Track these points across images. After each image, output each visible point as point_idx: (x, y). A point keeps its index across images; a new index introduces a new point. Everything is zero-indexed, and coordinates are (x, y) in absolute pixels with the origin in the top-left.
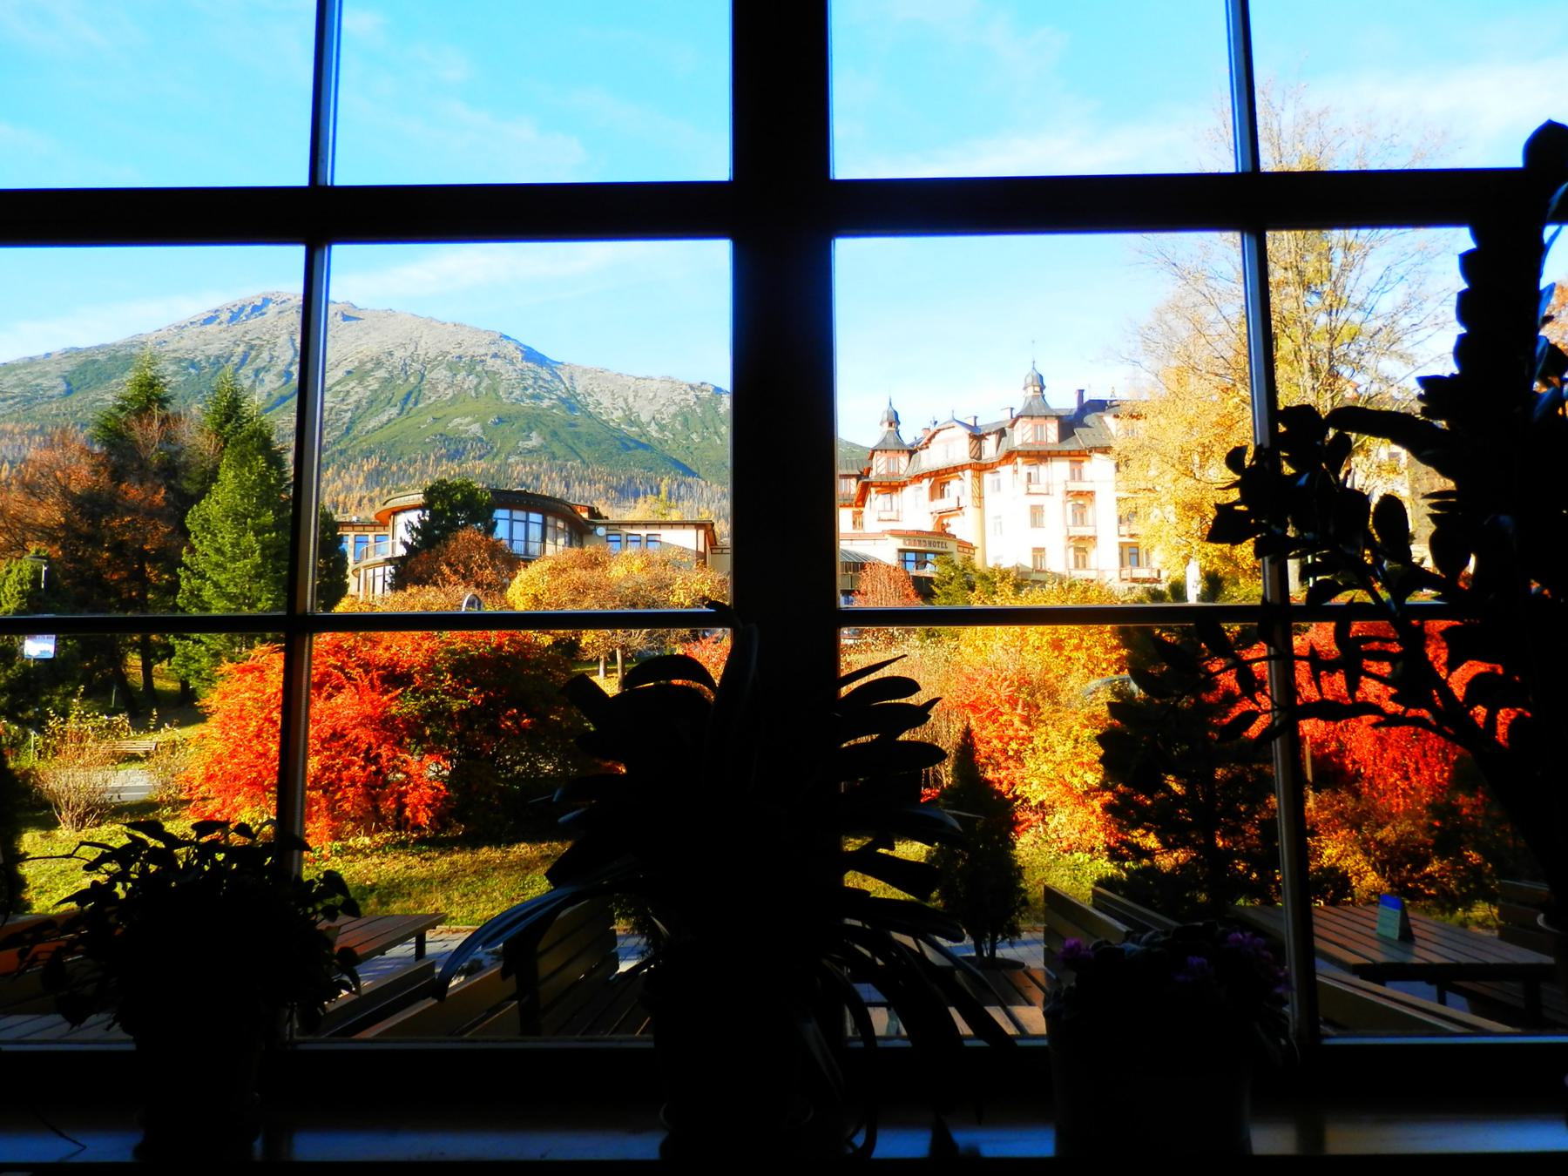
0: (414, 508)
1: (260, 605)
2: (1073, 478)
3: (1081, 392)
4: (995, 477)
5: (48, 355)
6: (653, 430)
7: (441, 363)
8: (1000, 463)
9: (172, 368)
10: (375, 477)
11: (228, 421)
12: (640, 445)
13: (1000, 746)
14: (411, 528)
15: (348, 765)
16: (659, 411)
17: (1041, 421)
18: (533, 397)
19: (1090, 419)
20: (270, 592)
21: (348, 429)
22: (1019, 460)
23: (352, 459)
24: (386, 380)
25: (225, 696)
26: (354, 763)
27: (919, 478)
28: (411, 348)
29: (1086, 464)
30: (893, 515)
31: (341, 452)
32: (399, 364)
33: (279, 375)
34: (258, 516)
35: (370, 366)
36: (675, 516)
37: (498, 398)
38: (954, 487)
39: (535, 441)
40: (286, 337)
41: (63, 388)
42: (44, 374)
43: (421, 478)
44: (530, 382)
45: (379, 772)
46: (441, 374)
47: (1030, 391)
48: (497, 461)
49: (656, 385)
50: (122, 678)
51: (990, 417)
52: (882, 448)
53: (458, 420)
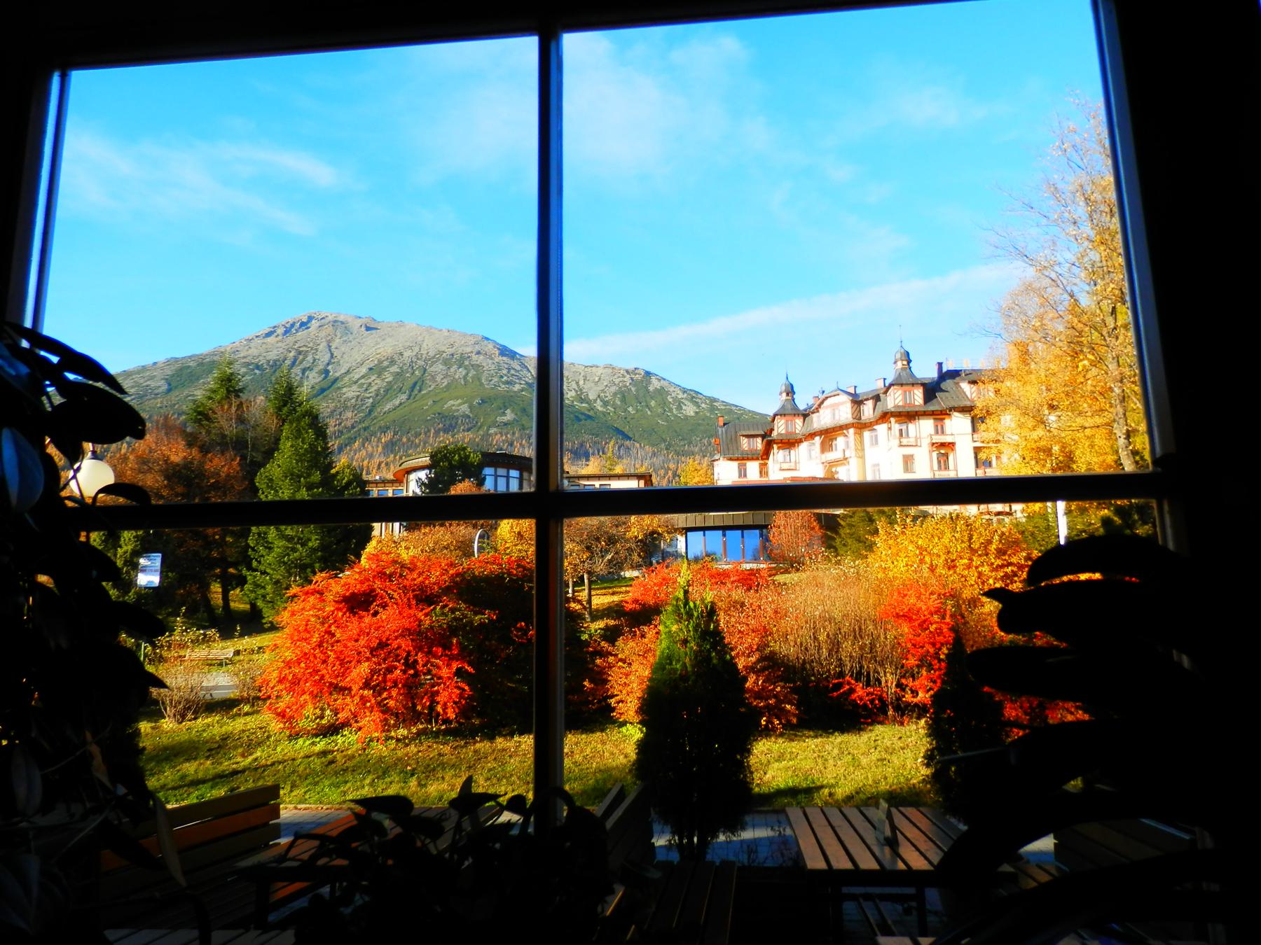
0: (422, 468)
1: (310, 544)
2: (937, 433)
3: (940, 365)
4: (874, 434)
5: (155, 364)
6: (599, 406)
7: (438, 359)
8: (877, 422)
9: (243, 370)
10: (390, 447)
11: (285, 405)
12: (589, 417)
13: (932, 650)
14: (421, 483)
15: (390, 670)
16: (603, 391)
17: (910, 387)
18: (507, 383)
19: (947, 385)
20: (317, 534)
21: (370, 412)
22: (892, 420)
23: (373, 434)
24: (398, 374)
25: (293, 614)
26: (396, 668)
27: (812, 436)
28: (416, 349)
29: (947, 421)
30: (792, 465)
31: (365, 429)
32: (407, 361)
33: (320, 373)
34: (309, 475)
35: (386, 363)
36: (618, 470)
37: (482, 384)
38: (840, 442)
39: (509, 416)
40: (324, 344)
41: (165, 387)
42: (152, 378)
43: (424, 447)
44: (505, 372)
45: (416, 675)
46: (439, 367)
47: (900, 364)
48: (481, 432)
49: (600, 371)
50: (207, 601)
51: (866, 386)
52: (780, 414)
53: (452, 402)
